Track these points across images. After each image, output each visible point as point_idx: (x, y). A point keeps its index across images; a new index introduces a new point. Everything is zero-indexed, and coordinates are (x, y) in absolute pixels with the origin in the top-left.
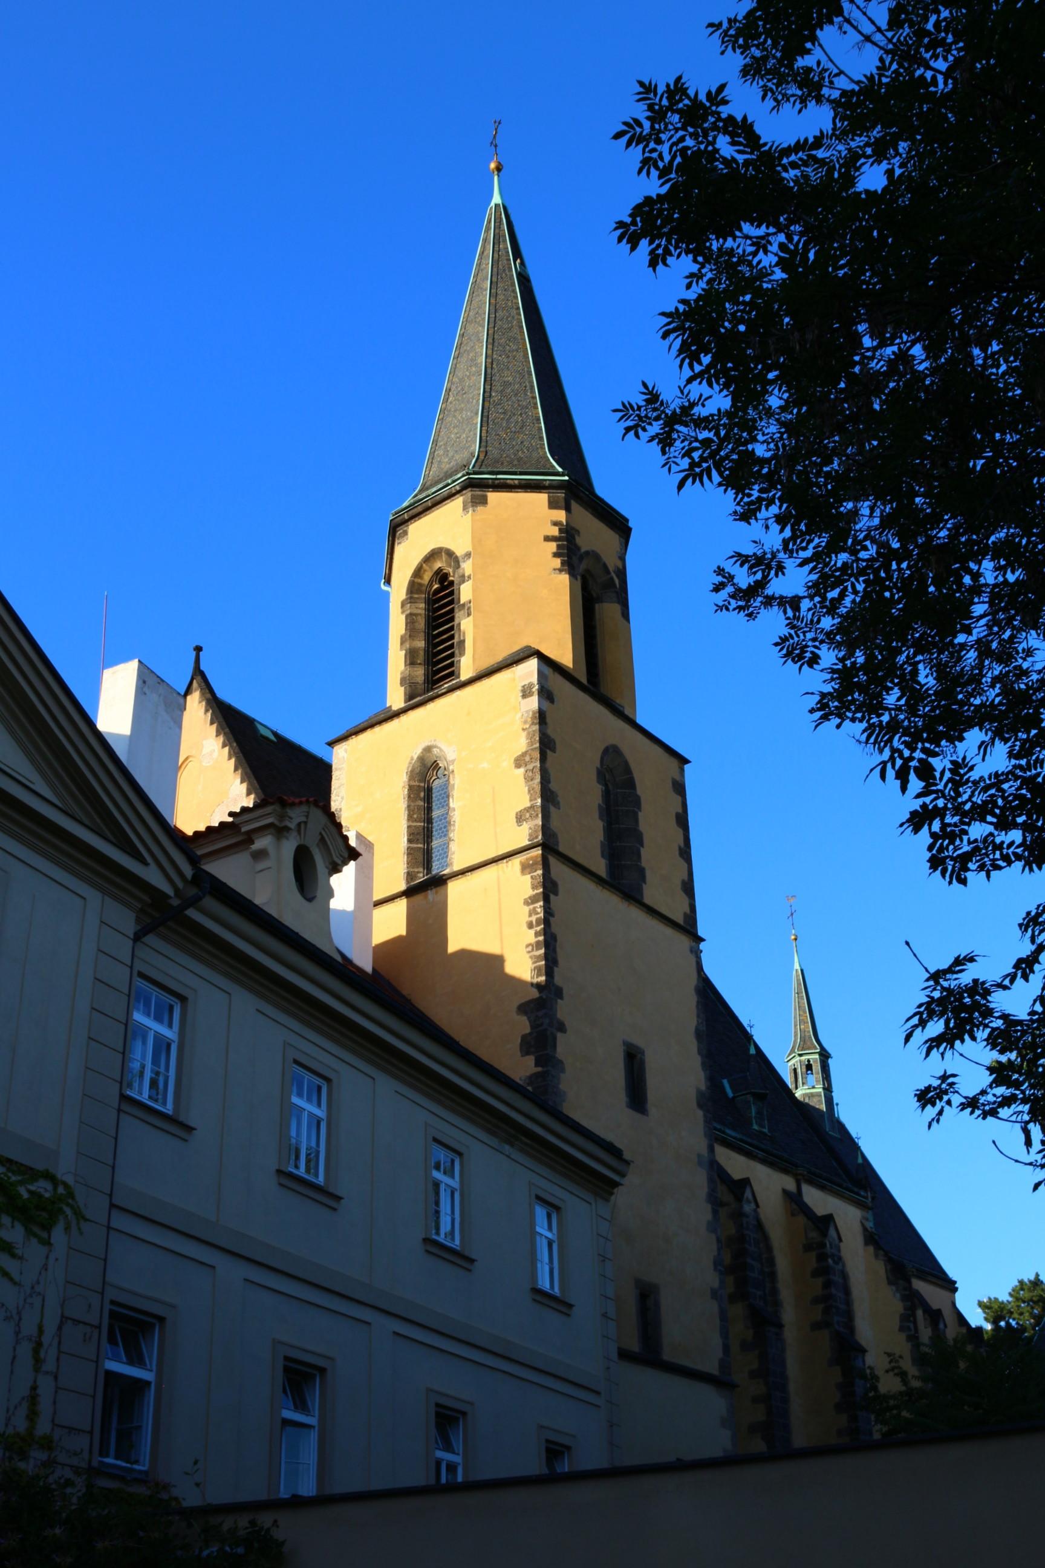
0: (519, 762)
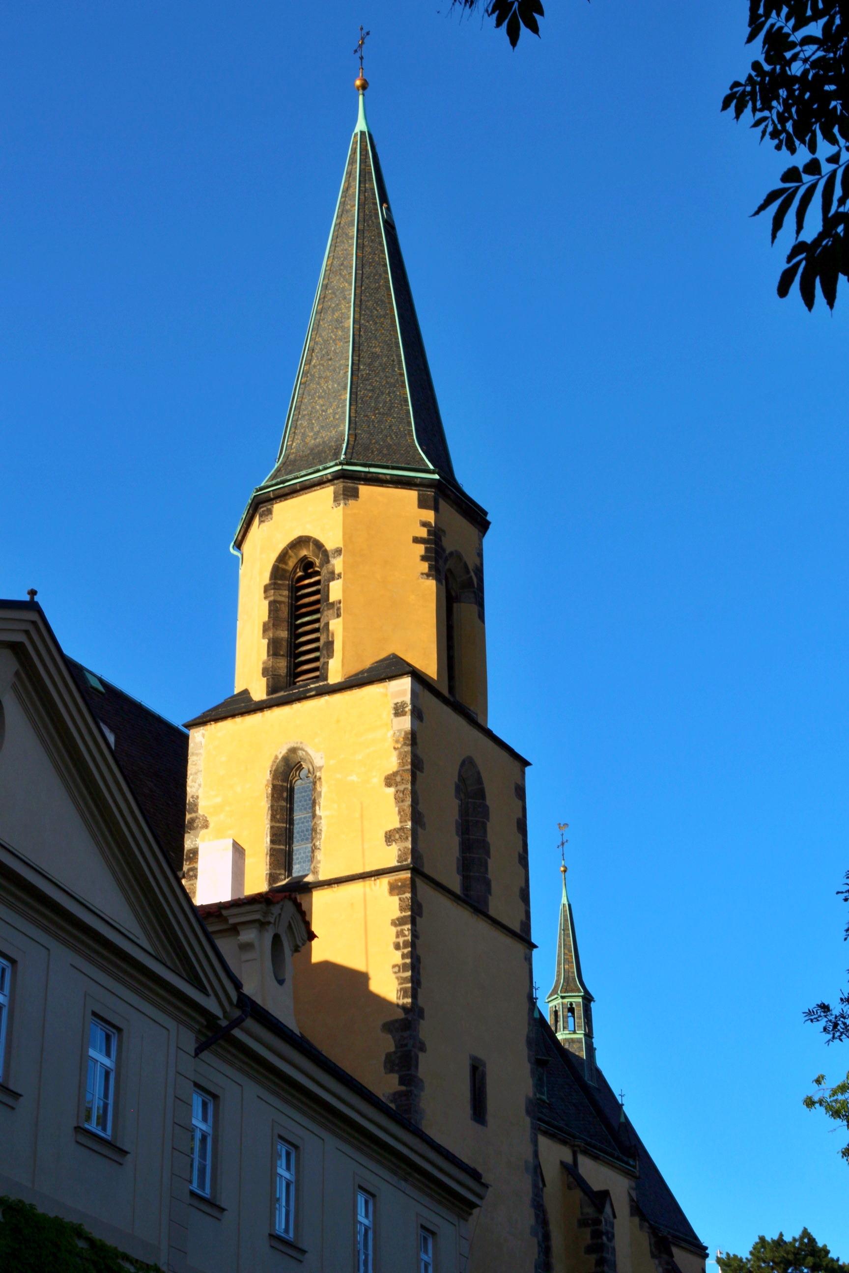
0: (389, 781)
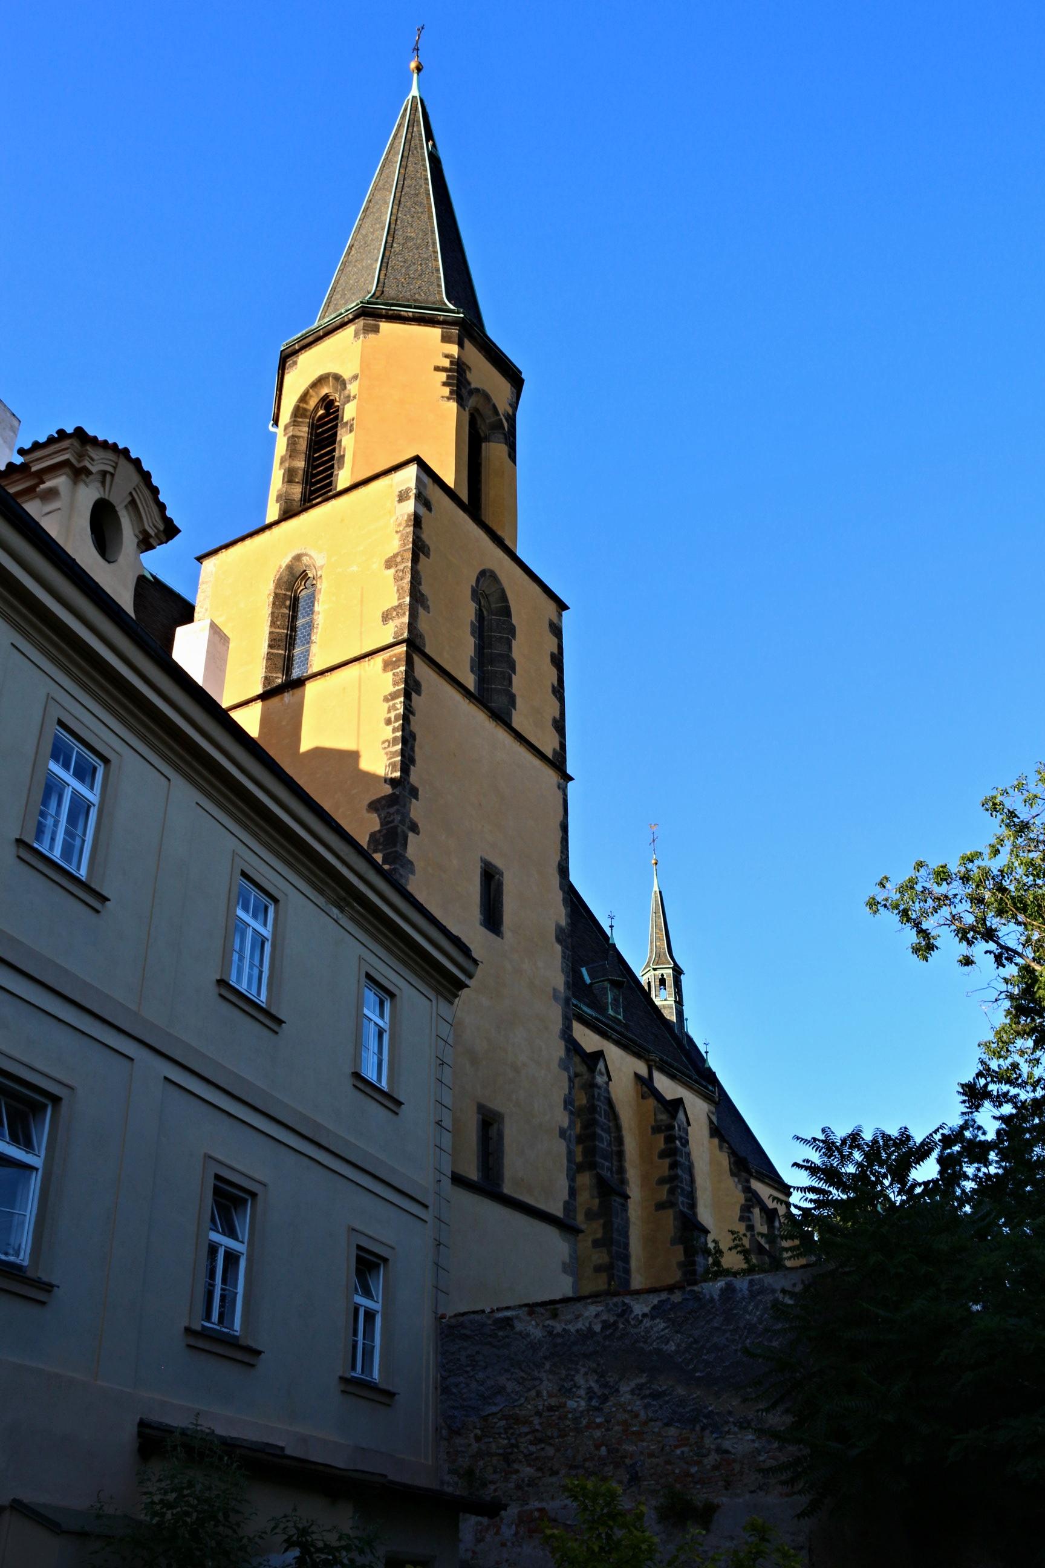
0: (389, 563)
